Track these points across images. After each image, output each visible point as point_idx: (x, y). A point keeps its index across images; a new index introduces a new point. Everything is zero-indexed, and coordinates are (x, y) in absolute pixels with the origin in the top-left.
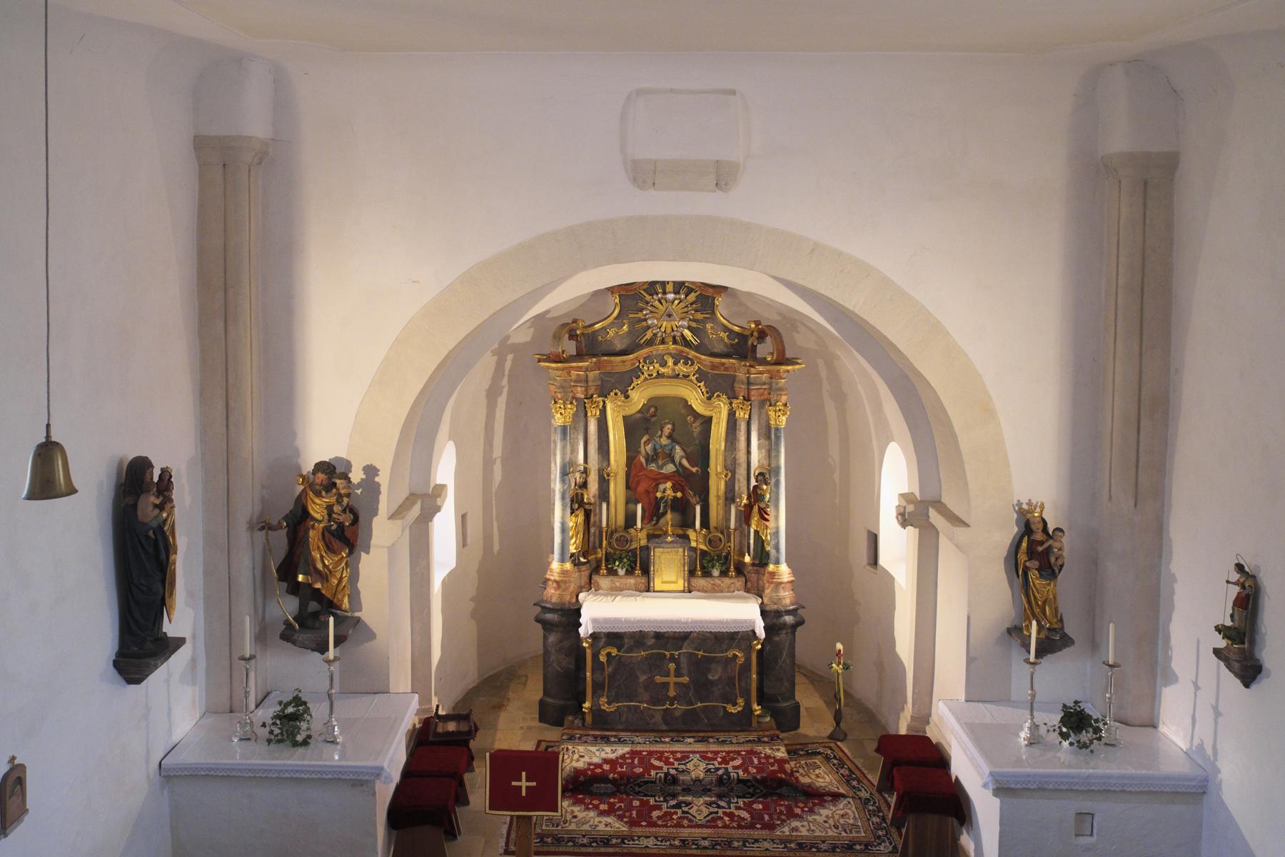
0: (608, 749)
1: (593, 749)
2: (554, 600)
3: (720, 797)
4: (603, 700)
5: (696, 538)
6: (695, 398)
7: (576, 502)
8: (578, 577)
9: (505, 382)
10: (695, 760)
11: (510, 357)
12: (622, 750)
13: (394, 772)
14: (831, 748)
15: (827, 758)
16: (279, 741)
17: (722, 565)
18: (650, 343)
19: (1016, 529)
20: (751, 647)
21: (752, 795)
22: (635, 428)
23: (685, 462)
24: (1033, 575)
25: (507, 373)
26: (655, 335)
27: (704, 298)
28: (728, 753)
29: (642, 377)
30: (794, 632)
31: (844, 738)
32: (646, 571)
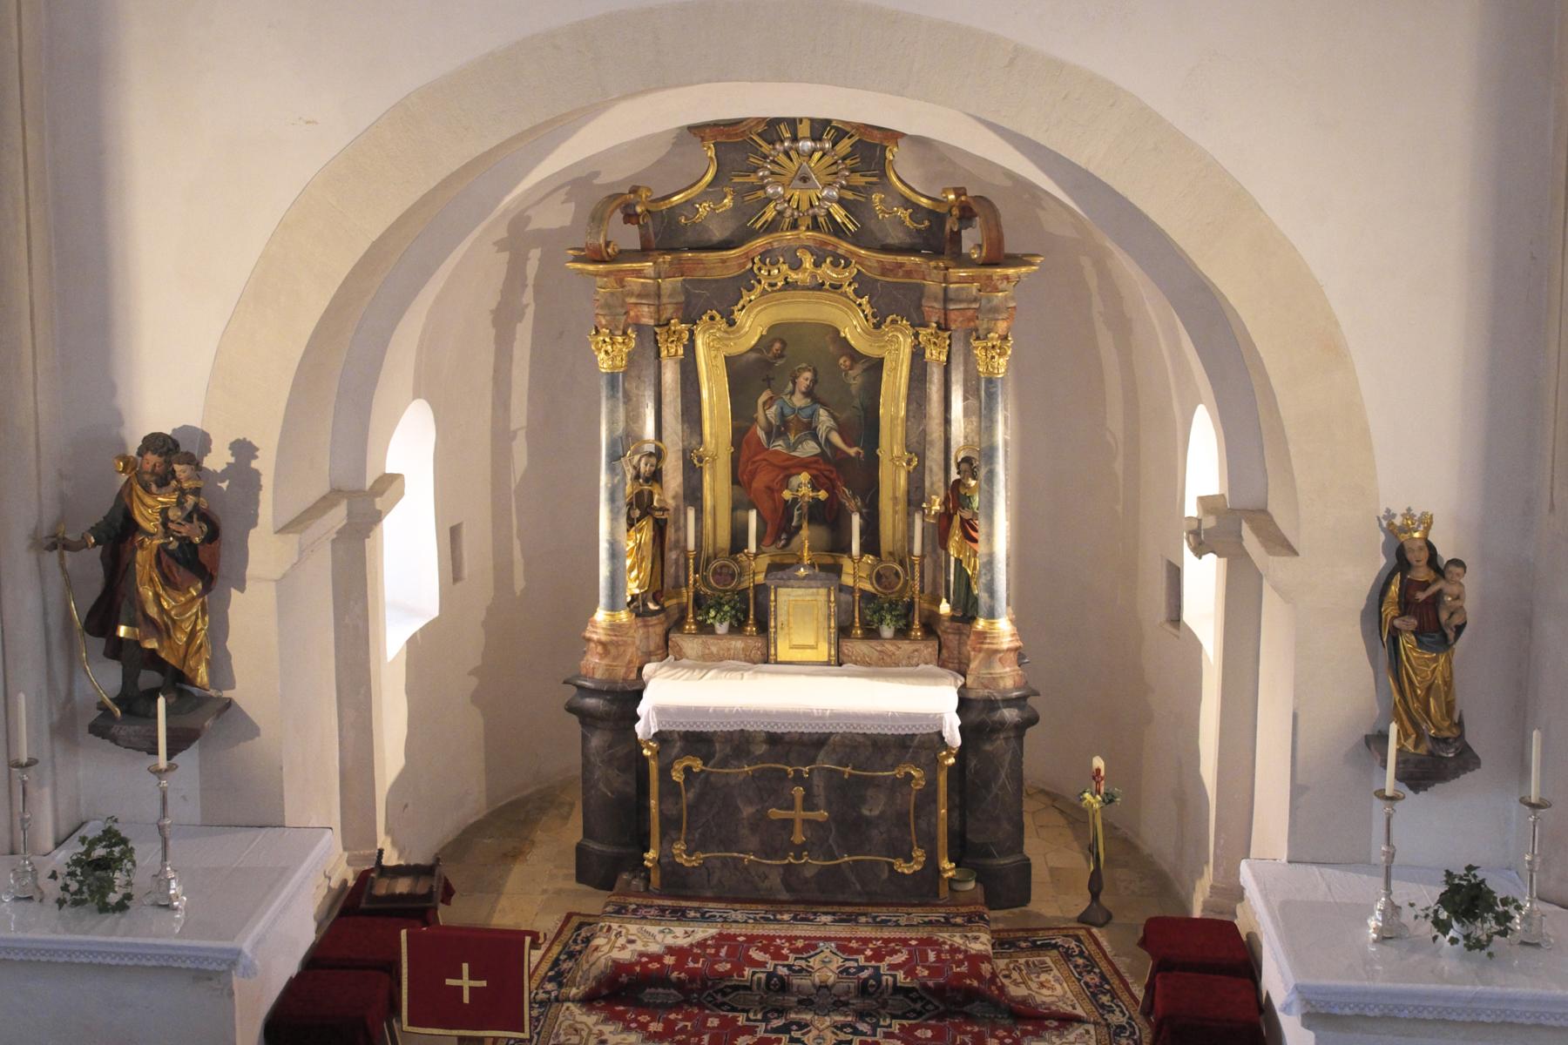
0: (679, 930)
1: (654, 930)
2: (598, 675)
3: (861, 1015)
4: (679, 847)
5: (856, 572)
6: (854, 327)
7: (640, 508)
8: (640, 638)
9: (528, 297)
10: (825, 951)
11: (535, 254)
12: (703, 932)
13: (285, 966)
14: (1078, 939)
15: (1067, 955)
16: (76, 903)
17: (898, 618)
18: (772, 227)
19: (1383, 561)
20: (936, 762)
21: (919, 1014)
22: (747, 377)
23: (836, 439)
24: (1407, 642)
25: (530, 282)
26: (780, 213)
27: (868, 149)
28: (887, 941)
29: (759, 288)
30: (1020, 737)
31: (1106, 920)
32: (763, 627)
